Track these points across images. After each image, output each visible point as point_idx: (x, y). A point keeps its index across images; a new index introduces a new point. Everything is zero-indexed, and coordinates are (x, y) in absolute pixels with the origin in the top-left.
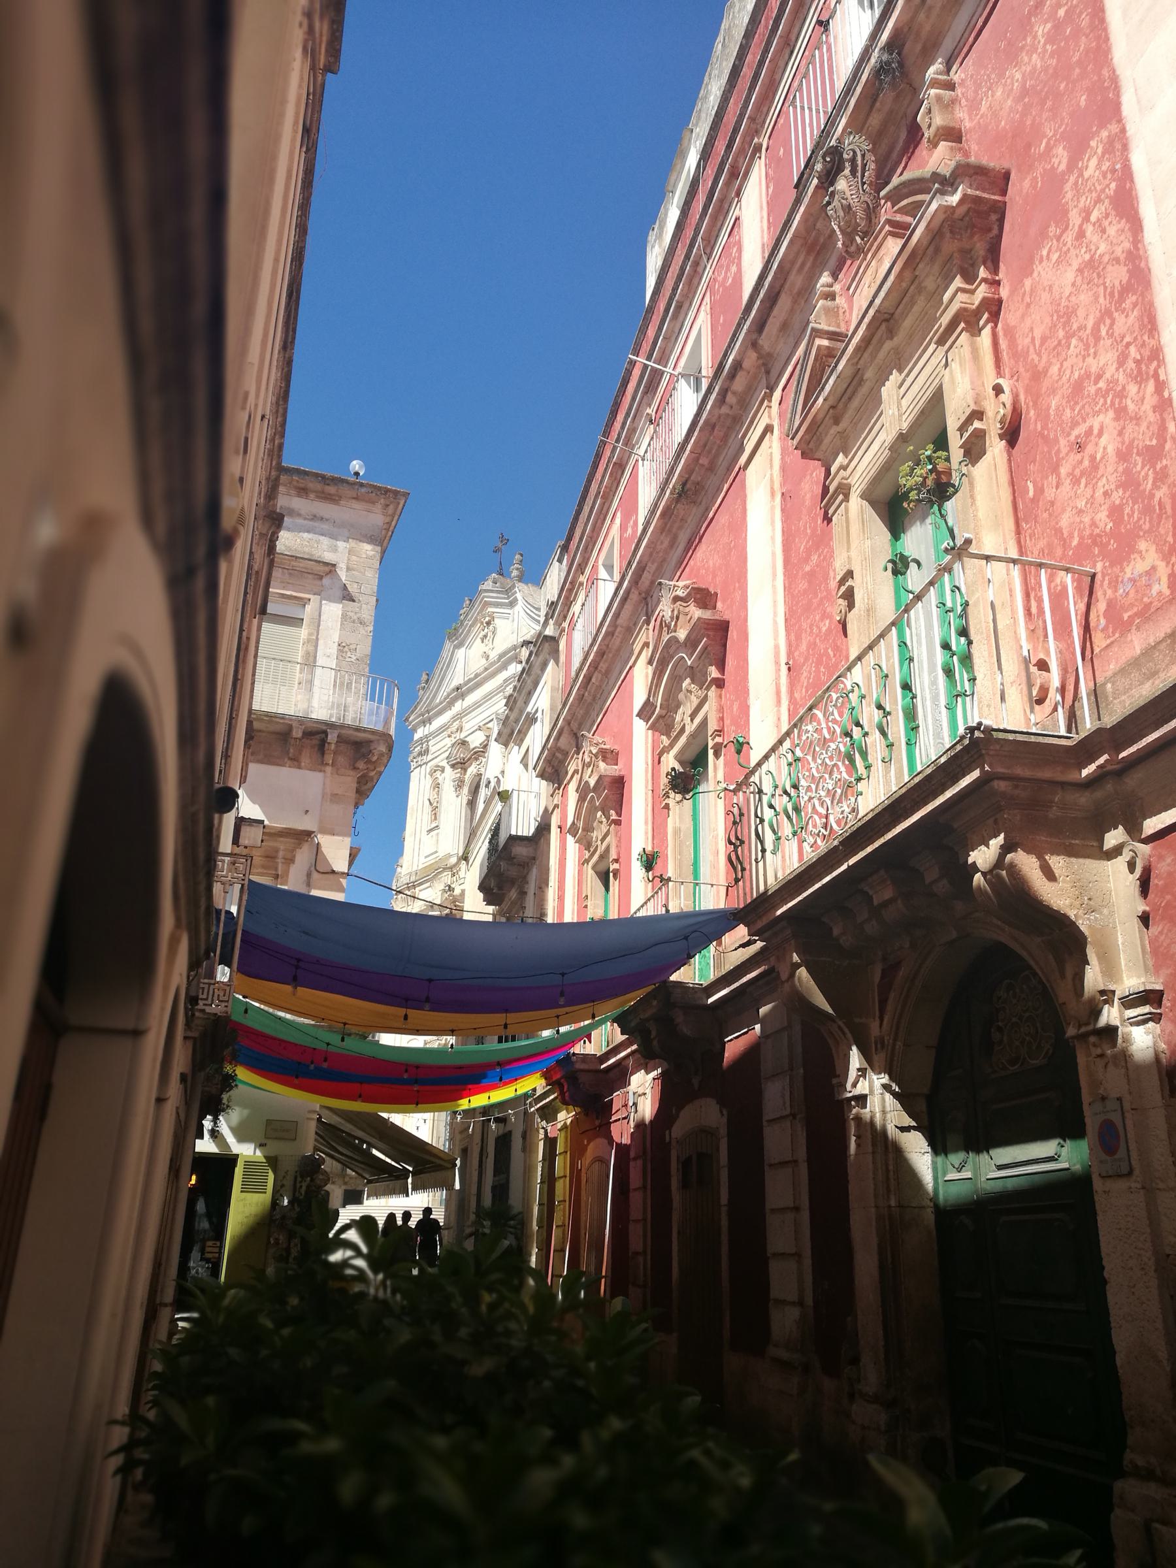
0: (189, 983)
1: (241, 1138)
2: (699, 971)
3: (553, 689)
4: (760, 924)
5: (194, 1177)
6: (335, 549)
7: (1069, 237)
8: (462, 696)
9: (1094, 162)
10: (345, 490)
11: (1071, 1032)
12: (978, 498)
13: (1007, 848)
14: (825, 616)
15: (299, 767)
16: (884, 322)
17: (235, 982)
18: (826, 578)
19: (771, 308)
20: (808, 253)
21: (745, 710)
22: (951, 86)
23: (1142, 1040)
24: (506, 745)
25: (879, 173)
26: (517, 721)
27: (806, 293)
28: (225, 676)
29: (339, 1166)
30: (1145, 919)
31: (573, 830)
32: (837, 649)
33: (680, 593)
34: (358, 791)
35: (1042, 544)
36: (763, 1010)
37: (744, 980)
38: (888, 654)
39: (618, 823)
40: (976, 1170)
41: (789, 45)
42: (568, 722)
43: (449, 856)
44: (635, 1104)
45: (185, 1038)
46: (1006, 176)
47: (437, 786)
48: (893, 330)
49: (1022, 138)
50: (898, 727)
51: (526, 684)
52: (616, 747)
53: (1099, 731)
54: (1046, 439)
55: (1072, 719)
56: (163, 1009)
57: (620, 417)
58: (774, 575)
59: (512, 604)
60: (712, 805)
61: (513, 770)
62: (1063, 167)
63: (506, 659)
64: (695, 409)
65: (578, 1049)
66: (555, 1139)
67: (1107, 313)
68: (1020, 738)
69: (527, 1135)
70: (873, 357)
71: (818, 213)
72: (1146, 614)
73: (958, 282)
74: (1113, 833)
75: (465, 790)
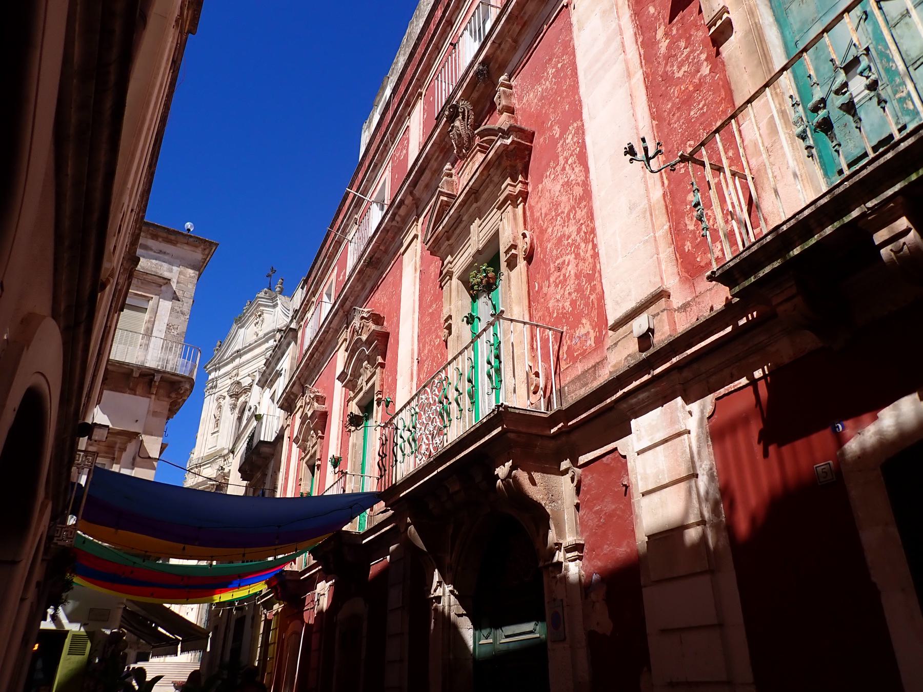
0: (49, 528)
1: (71, 620)
2: (357, 525)
3: (293, 358)
4: (391, 502)
5: (37, 645)
6: (171, 271)
7: (559, 168)
8: (240, 356)
9: (570, 137)
10: (180, 238)
11: (541, 564)
12: (512, 287)
13: (513, 468)
14: (437, 336)
15: (135, 394)
16: (474, 193)
17: (79, 525)
18: (440, 317)
19: (421, 176)
20: (441, 152)
21: (395, 381)
22: (510, 87)
23: (574, 570)
24: (263, 388)
25: (475, 120)
26: (270, 374)
27: (439, 170)
28: (93, 351)
29: (136, 637)
30: (577, 507)
31: (296, 441)
32: (442, 354)
33: (365, 315)
34: (170, 410)
35: (540, 314)
36: (392, 548)
37: (383, 531)
38: (463, 364)
39: (322, 438)
40: (495, 639)
41: (438, 48)
42: (299, 378)
43: (224, 449)
44: (318, 600)
45: (43, 560)
46: (534, 133)
47: (220, 407)
48: (478, 199)
49: (540, 118)
50: (466, 402)
51: (277, 353)
52: (325, 395)
53: (559, 411)
54: (544, 262)
55: (549, 403)
56: (31, 547)
57: (341, 217)
58: (414, 312)
59: (275, 306)
60: (374, 434)
61: (265, 402)
62: (557, 136)
63: (267, 337)
64: (380, 219)
65: (287, 568)
66: (271, 620)
67: (573, 208)
68: (522, 412)
69: (255, 618)
70: (467, 210)
71: (445, 134)
72: (584, 355)
73: (508, 181)
74: (565, 462)
75: (237, 410)
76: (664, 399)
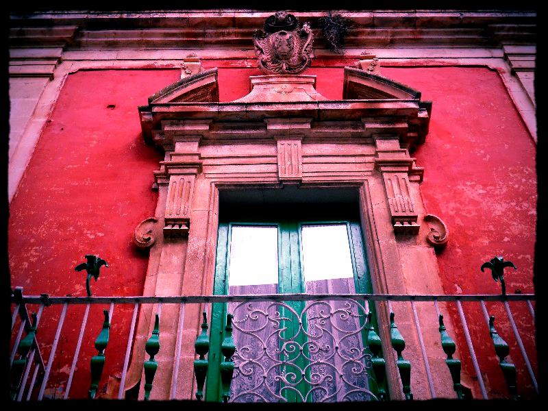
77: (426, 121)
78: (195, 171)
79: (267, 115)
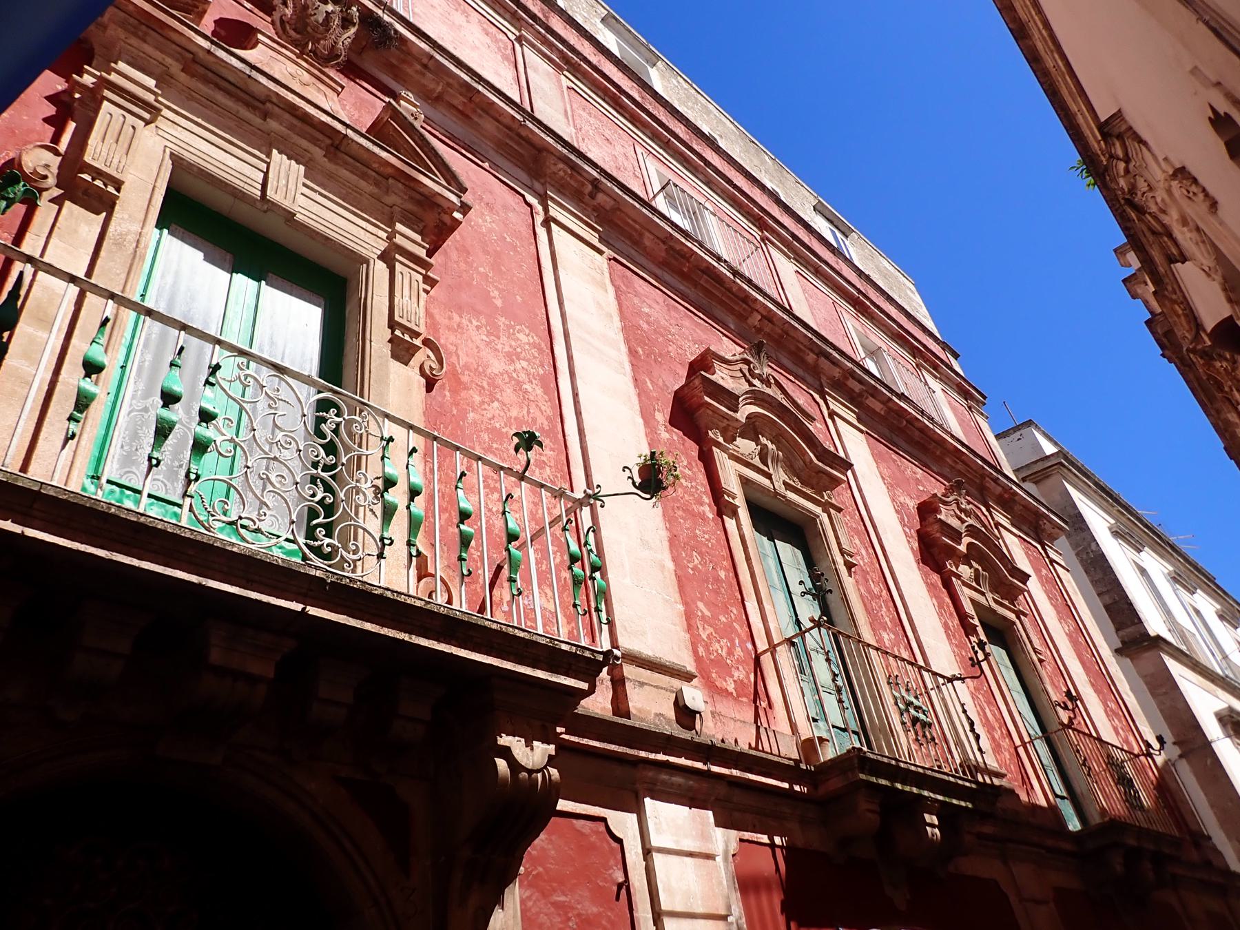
76: (693, 801)
77: (458, 223)
78: (147, 116)
79: (275, 100)
